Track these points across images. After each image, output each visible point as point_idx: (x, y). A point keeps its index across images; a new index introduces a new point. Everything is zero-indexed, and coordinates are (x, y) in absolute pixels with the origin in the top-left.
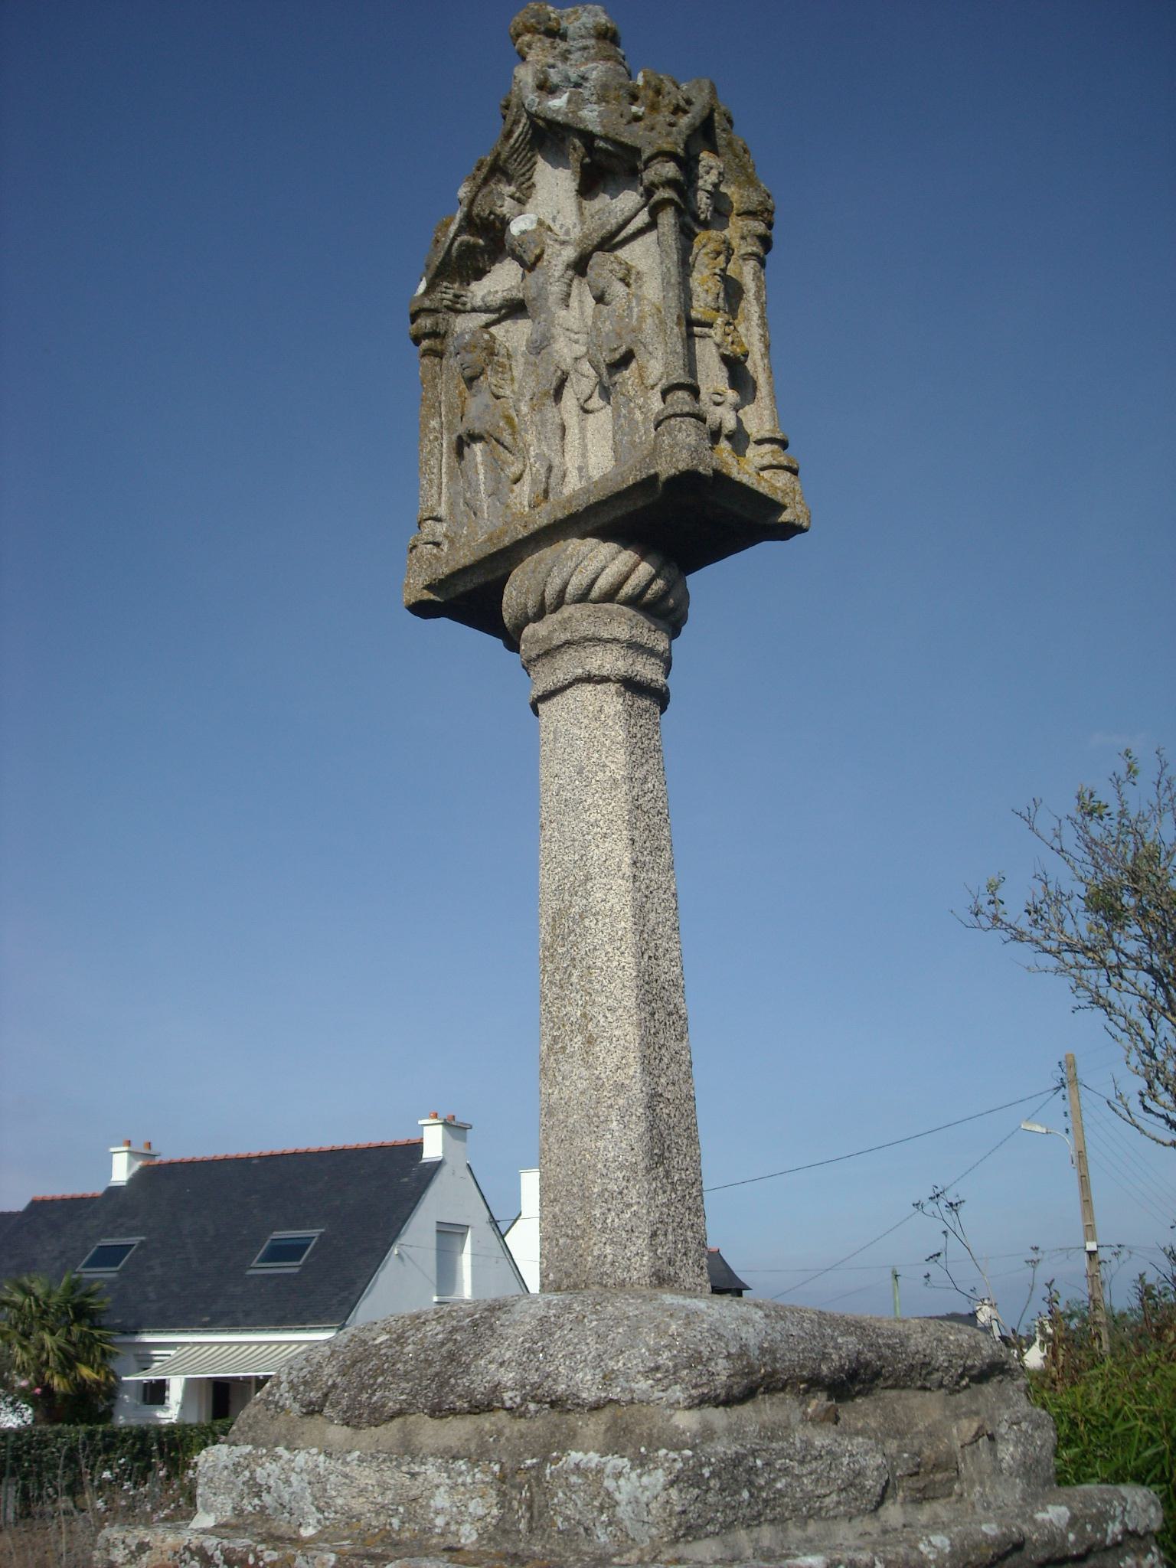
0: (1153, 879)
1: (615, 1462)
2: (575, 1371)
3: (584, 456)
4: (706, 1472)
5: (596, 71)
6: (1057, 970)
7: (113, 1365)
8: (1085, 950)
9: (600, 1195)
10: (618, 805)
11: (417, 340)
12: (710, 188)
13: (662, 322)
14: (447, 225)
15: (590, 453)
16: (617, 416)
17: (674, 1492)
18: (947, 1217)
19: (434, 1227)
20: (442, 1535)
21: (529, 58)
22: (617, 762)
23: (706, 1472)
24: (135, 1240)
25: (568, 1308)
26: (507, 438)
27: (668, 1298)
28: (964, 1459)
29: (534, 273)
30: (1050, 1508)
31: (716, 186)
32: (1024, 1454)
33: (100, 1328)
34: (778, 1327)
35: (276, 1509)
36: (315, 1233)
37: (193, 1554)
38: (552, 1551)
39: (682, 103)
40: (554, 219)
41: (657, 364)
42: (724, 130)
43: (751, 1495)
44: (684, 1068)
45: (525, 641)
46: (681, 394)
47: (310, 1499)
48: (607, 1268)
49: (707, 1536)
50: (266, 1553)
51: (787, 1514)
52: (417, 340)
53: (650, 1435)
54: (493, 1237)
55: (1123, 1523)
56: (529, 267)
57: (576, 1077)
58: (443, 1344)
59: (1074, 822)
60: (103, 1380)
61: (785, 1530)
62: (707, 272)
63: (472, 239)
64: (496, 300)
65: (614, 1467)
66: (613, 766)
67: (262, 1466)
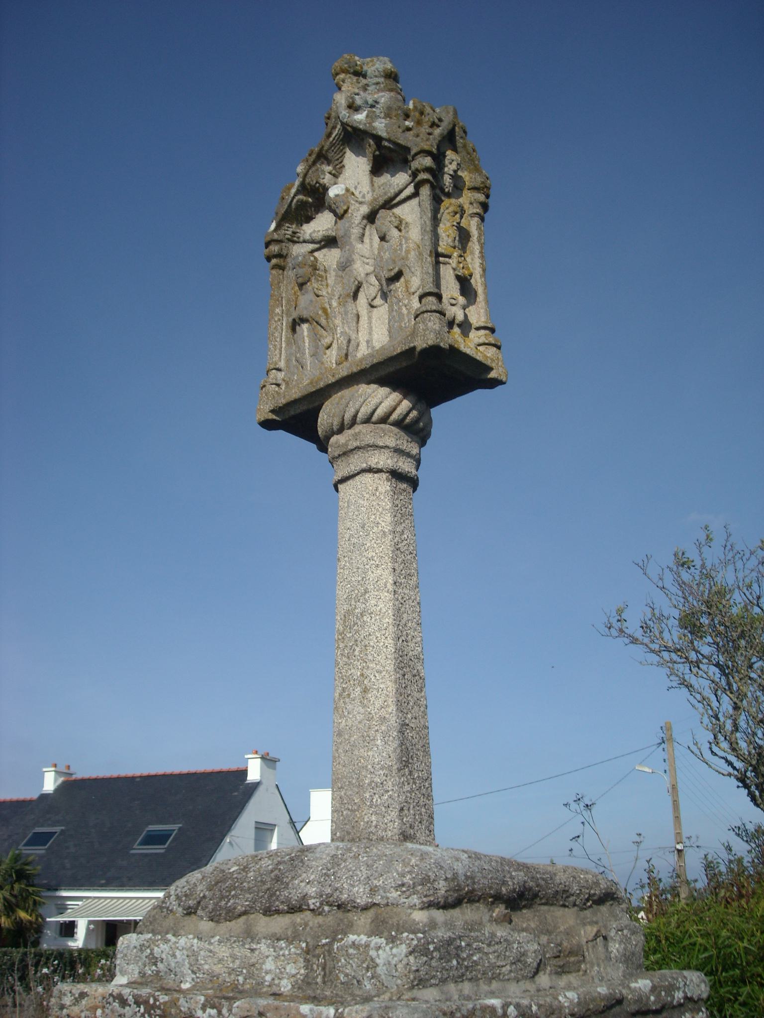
0: (721, 607)
1: (376, 940)
2: (353, 886)
3: (370, 334)
4: (431, 947)
5: (384, 98)
6: (659, 665)
7: (41, 911)
8: (676, 651)
9: (370, 784)
10: (385, 547)
11: (269, 259)
12: (452, 173)
13: (420, 254)
14: (289, 189)
15: (375, 332)
16: (391, 310)
17: (411, 958)
18: (584, 813)
19: (253, 825)
20: (269, 986)
21: (343, 89)
22: (386, 521)
23: (431, 947)
24: (58, 829)
25: (349, 850)
26: (323, 321)
27: (409, 845)
28: (588, 950)
29: (342, 221)
30: (639, 981)
31: (455, 171)
32: (625, 949)
33: (33, 886)
34: (476, 864)
35: (166, 972)
36: (176, 827)
37: (115, 998)
38: (337, 994)
39: (436, 121)
40: (356, 188)
41: (417, 279)
42: (462, 137)
43: (458, 963)
44: (422, 709)
45: (332, 446)
46: (431, 298)
47: (188, 966)
48: (373, 829)
49: (431, 986)
50: (161, 997)
51: (479, 976)
52: (269, 259)
53: (398, 924)
54: (292, 832)
55: (684, 992)
56: (340, 217)
57: (356, 713)
58: (272, 871)
59: (671, 570)
60: (34, 920)
61: (478, 985)
62: (448, 224)
63: (305, 198)
64: (318, 236)
65: (376, 943)
66: (383, 524)
67: (158, 946)
